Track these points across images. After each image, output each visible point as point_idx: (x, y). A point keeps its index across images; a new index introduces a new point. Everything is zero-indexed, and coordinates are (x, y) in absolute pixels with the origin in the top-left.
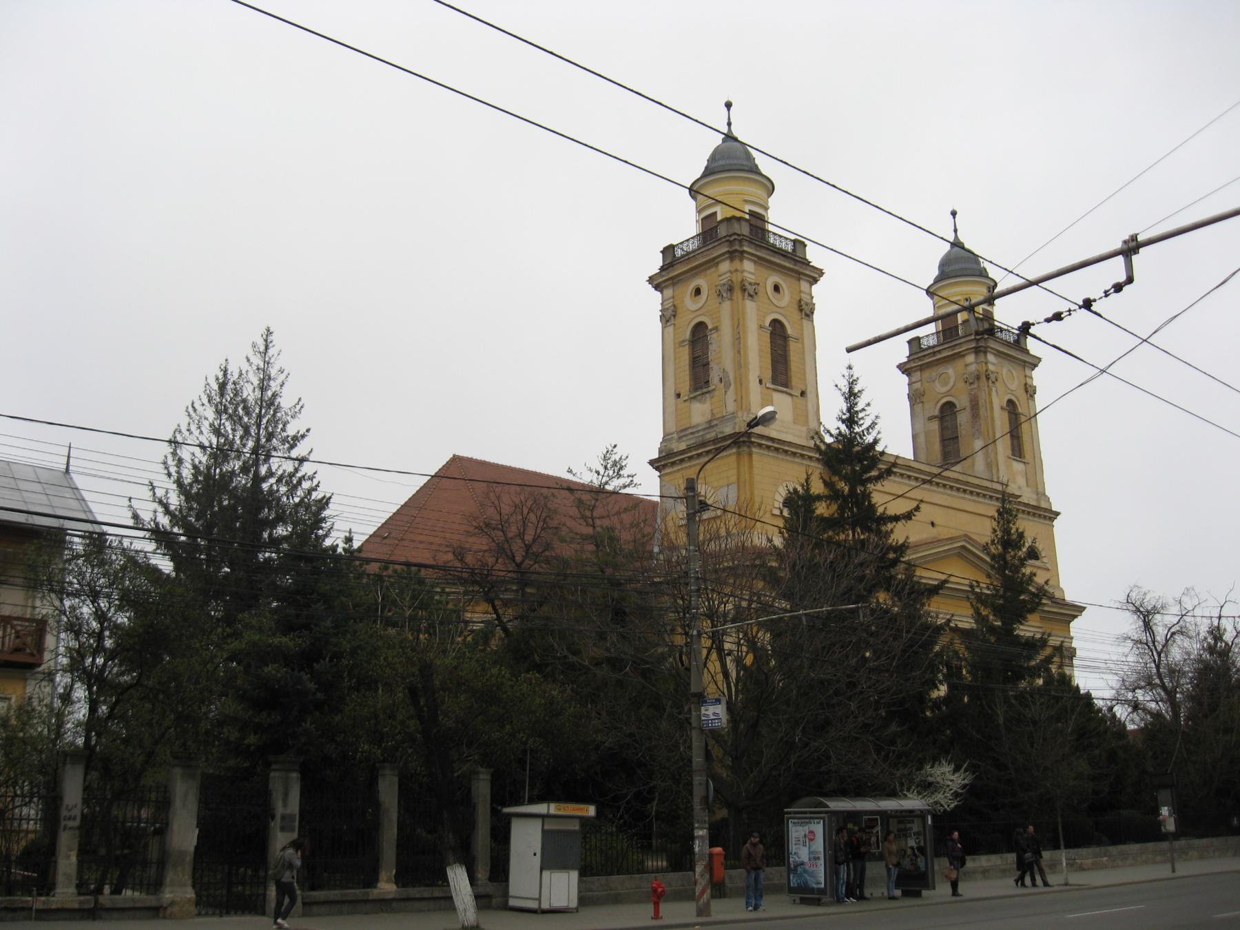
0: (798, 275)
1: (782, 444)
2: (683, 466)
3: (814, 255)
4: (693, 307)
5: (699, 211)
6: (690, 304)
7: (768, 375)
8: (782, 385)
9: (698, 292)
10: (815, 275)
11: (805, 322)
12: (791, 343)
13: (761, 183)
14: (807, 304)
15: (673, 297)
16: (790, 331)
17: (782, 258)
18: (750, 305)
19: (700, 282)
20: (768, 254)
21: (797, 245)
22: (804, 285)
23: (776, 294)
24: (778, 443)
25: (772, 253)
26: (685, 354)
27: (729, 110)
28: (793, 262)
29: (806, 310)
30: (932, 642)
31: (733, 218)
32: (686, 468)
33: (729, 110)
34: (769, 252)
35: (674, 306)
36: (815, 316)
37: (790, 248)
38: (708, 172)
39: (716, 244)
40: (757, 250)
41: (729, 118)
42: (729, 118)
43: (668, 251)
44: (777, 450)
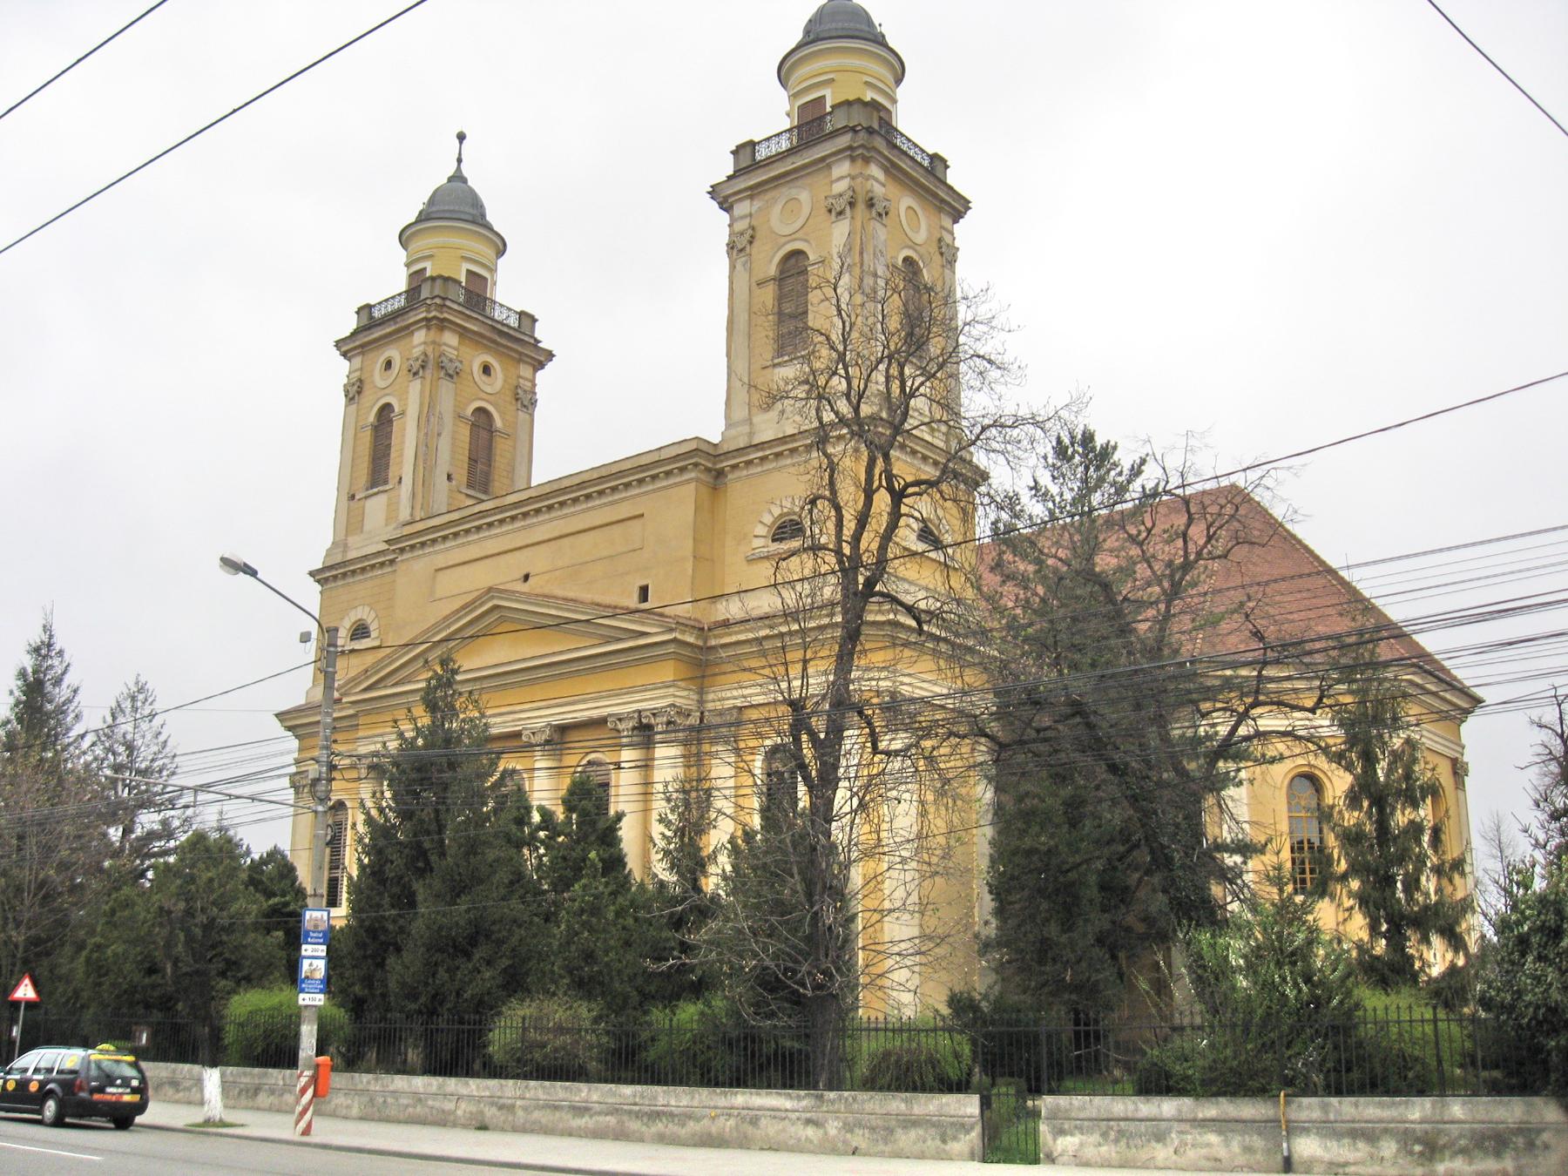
0: (520, 359)
3: (545, 335)
4: (381, 384)
5: (408, 265)
6: (379, 379)
7: (461, 476)
9: (389, 365)
10: (542, 357)
11: (522, 415)
12: (498, 439)
13: (885, 61)
14: (948, 245)
15: (361, 369)
16: (498, 423)
18: (446, 389)
19: (393, 352)
21: (937, 162)
22: (525, 371)
23: (484, 378)
26: (367, 437)
27: (461, 143)
29: (525, 401)
33: (461, 143)
35: (753, 229)
36: (958, 265)
37: (513, 321)
38: (423, 217)
41: (460, 154)
42: (460, 154)
43: (744, 151)
44: (344, 575)
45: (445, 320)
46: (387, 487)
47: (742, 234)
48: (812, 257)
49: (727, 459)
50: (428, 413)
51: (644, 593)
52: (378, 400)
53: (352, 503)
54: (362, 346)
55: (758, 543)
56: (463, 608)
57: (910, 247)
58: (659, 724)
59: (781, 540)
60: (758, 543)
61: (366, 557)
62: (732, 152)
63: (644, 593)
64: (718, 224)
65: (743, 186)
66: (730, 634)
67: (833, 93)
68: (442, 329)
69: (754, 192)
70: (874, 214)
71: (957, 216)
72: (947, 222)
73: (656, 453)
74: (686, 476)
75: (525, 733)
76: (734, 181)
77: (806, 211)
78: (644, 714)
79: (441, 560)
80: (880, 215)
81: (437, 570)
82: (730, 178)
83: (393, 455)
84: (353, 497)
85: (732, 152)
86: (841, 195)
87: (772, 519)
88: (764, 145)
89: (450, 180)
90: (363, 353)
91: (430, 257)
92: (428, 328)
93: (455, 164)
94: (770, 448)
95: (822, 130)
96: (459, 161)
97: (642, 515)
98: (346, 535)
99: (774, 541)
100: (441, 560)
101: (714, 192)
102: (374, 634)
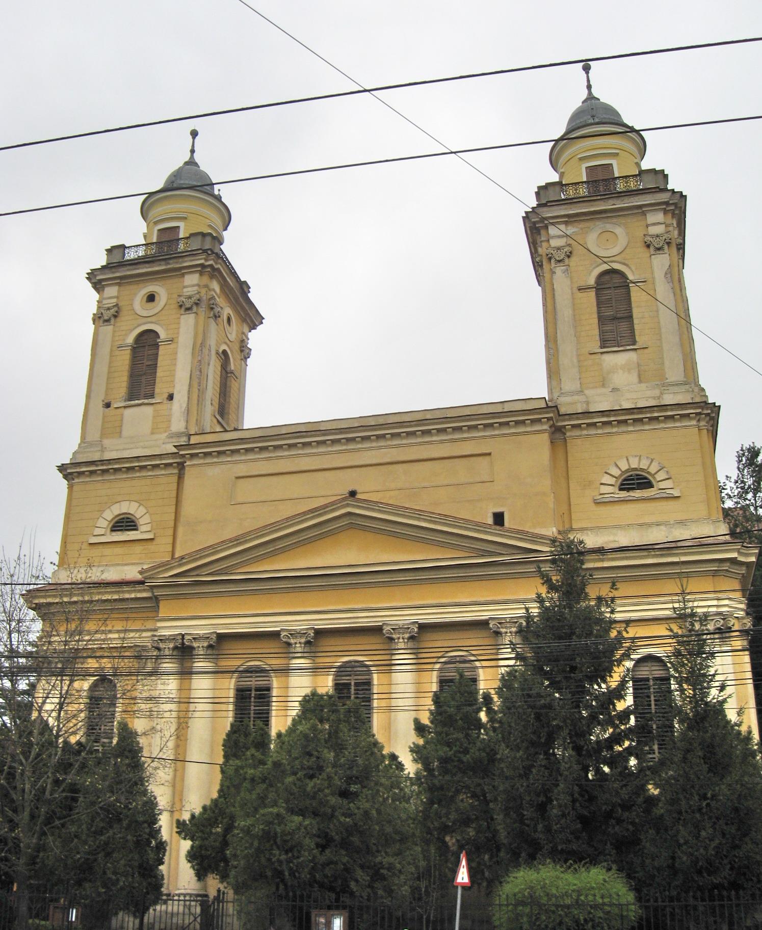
1: (110, 464)
2: (234, 459)
8: (146, 397)
9: (151, 298)
15: (117, 297)
17: (147, 265)
19: (160, 290)
20: (128, 270)
24: (102, 465)
25: (134, 267)
27: (587, 73)
28: (163, 263)
30: (607, 631)
31: (210, 234)
32: (194, 465)
33: (587, 73)
34: (129, 267)
39: (599, 198)
40: (113, 273)
41: (588, 81)
42: (588, 81)
44: (104, 471)
45: (218, 270)
46: (153, 401)
47: (109, 309)
48: (163, 335)
49: (569, 420)
50: (199, 347)
51: (499, 519)
52: (139, 325)
53: (107, 410)
54: (121, 278)
55: (604, 489)
56: (311, 511)
57: (226, 343)
58: (200, 647)
59: (628, 490)
60: (604, 489)
61: (137, 458)
62: (107, 250)
63: (499, 519)
64: (90, 299)
65: (563, 213)
66: (602, 560)
67: (185, 225)
68: (212, 277)
69: (121, 281)
70: (212, 315)
71: (253, 327)
72: (246, 329)
73: (501, 405)
74: (538, 427)
75: (283, 634)
76: (106, 271)
77: (162, 303)
78: (187, 637)
79: (242, 470)
80: (215, 317)
81: (238, 478)
82: (103, 267)
83: (160, 373)
84: (108, 405)
85: (107, 250)
86: (658, 236)
87: (620, 472)
88: (133, 250)
89: (186, 163)
90: (119, 284)
91: (616, 155)
92: (201, 274)
93: (586, 91)
94: (615, 415)
95: (177, 250)
96: (589, 87)
97: (489, 454)
98: (101, 438)
99: (621, 489)
100: (242, 470)
101: (92, 276)
102: (143, 528)
